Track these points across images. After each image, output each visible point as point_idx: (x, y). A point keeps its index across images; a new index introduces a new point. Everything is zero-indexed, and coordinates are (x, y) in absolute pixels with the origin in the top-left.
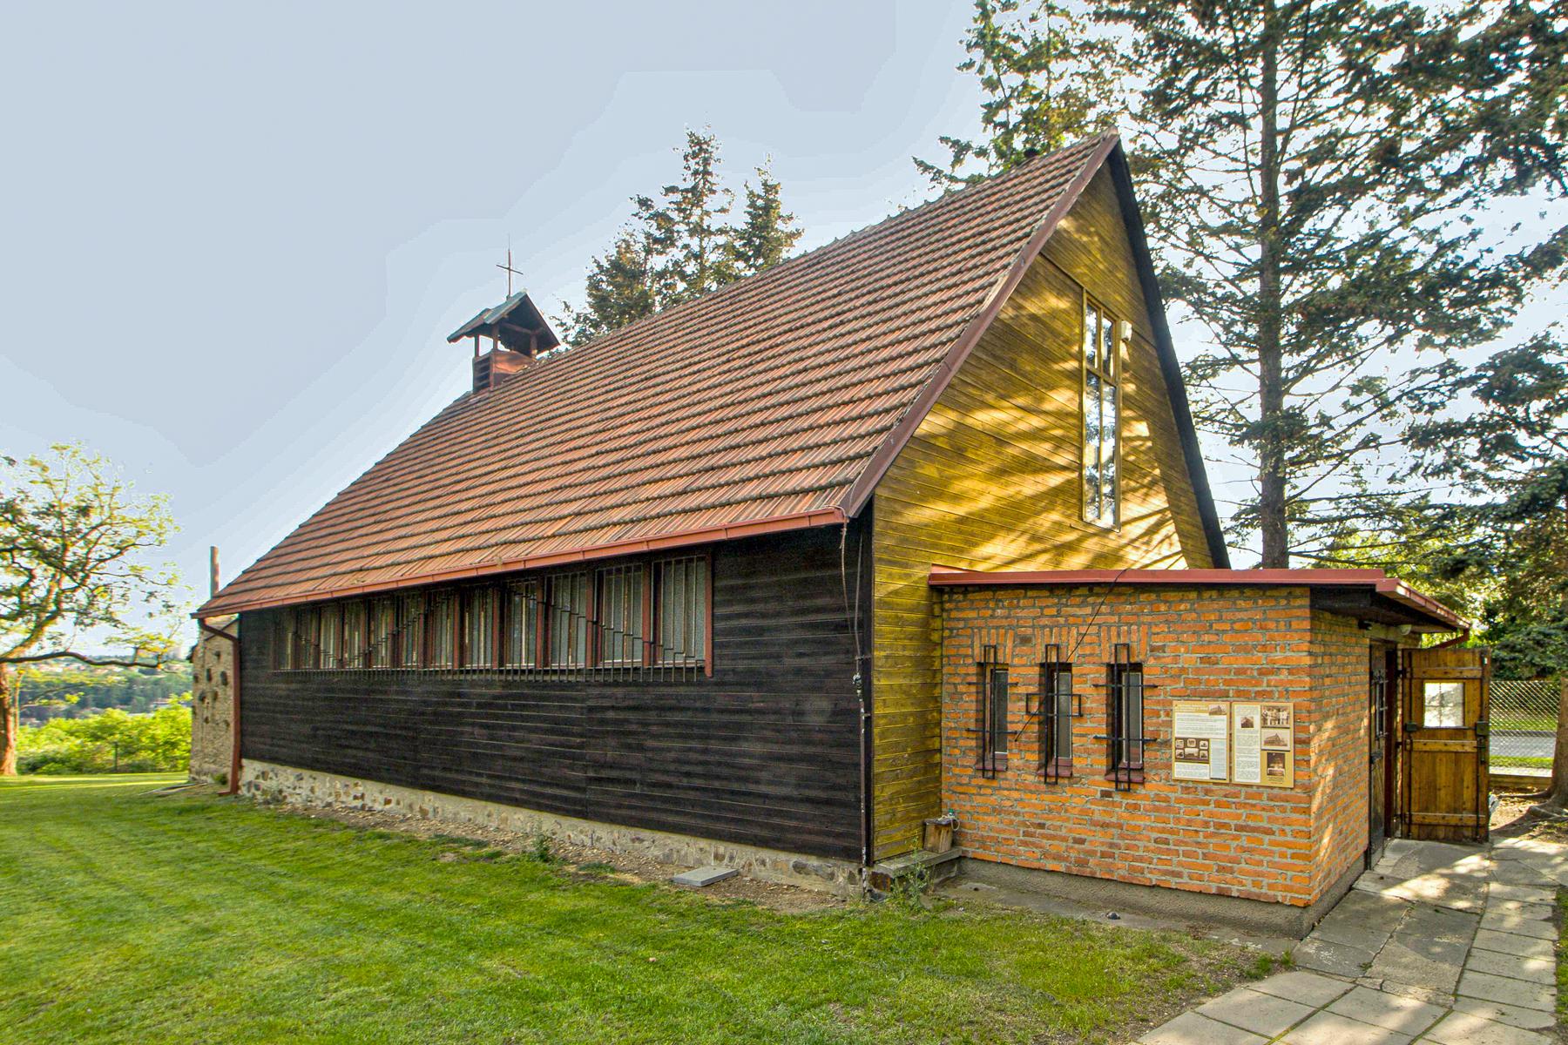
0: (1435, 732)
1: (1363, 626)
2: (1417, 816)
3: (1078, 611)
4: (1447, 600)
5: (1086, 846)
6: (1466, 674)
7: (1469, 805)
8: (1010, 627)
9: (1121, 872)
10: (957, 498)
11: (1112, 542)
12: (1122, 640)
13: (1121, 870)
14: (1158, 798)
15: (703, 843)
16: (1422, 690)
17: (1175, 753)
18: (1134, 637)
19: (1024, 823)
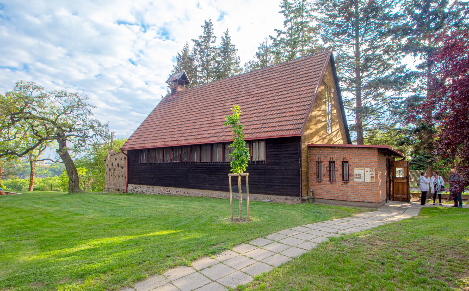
0: (398, 178)
1: (385, 155)
2: (395, 196)
3: (336, 152)
4: (401, 150)
5: (338, 194)
6: (404, 166)
7: (405, 194)
8: (323, 154)
9: (345, 199)
10: (311, 129)
11: (331, 136)
12: (345, 157)
13: (345, 198)
14: (352, 185)
15: (264, 195)
16: (396, 169)
17: (355, 177)
18: (347, 156)
19: (326, 191)
